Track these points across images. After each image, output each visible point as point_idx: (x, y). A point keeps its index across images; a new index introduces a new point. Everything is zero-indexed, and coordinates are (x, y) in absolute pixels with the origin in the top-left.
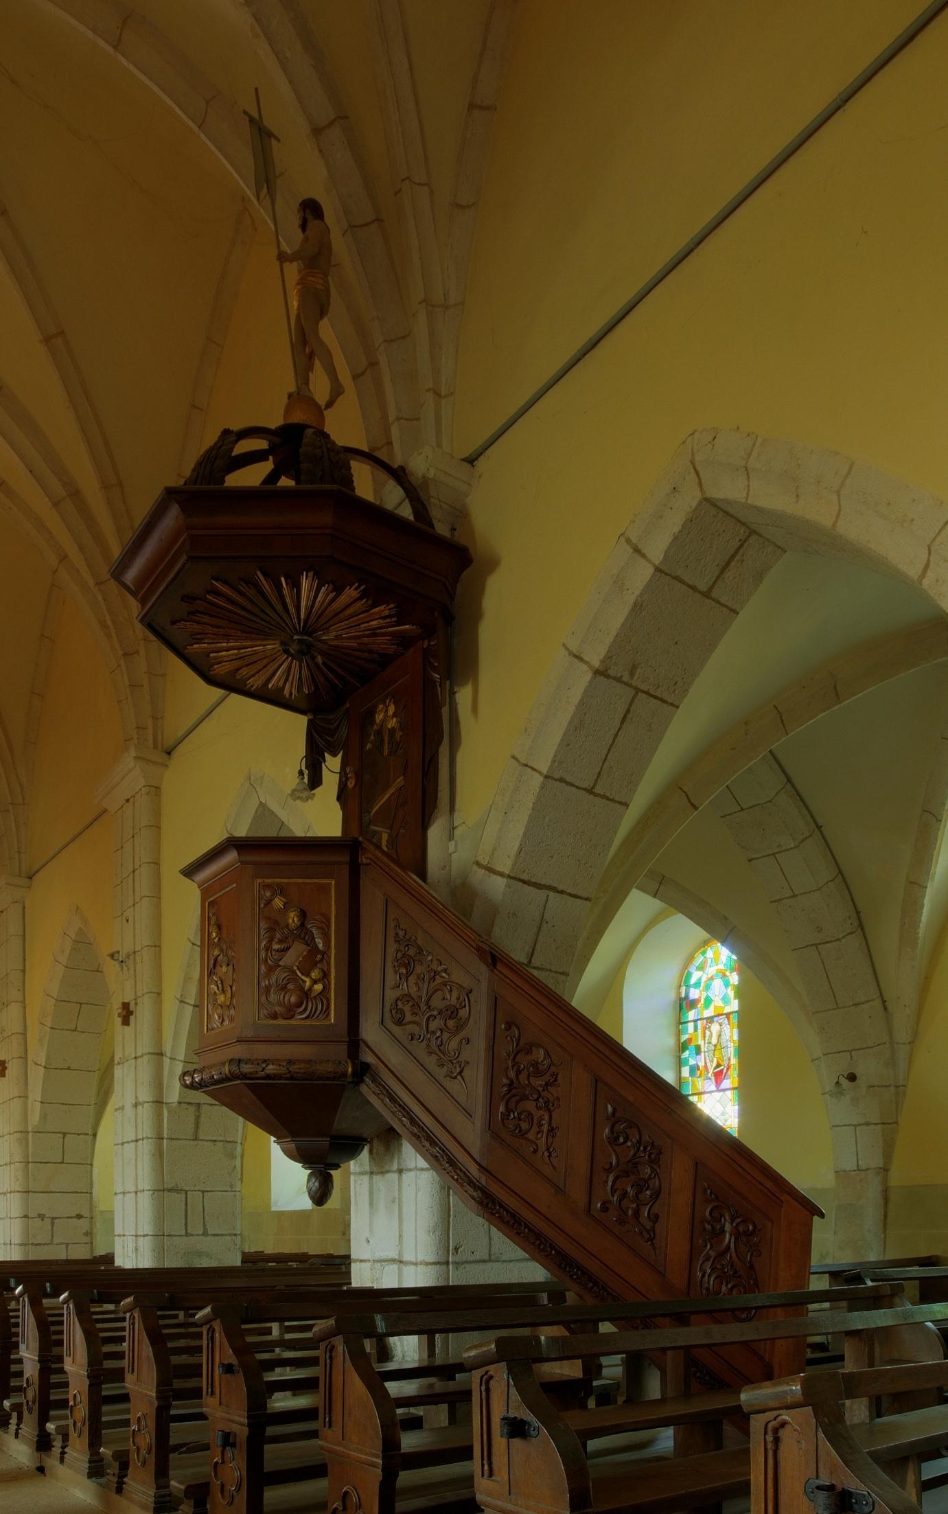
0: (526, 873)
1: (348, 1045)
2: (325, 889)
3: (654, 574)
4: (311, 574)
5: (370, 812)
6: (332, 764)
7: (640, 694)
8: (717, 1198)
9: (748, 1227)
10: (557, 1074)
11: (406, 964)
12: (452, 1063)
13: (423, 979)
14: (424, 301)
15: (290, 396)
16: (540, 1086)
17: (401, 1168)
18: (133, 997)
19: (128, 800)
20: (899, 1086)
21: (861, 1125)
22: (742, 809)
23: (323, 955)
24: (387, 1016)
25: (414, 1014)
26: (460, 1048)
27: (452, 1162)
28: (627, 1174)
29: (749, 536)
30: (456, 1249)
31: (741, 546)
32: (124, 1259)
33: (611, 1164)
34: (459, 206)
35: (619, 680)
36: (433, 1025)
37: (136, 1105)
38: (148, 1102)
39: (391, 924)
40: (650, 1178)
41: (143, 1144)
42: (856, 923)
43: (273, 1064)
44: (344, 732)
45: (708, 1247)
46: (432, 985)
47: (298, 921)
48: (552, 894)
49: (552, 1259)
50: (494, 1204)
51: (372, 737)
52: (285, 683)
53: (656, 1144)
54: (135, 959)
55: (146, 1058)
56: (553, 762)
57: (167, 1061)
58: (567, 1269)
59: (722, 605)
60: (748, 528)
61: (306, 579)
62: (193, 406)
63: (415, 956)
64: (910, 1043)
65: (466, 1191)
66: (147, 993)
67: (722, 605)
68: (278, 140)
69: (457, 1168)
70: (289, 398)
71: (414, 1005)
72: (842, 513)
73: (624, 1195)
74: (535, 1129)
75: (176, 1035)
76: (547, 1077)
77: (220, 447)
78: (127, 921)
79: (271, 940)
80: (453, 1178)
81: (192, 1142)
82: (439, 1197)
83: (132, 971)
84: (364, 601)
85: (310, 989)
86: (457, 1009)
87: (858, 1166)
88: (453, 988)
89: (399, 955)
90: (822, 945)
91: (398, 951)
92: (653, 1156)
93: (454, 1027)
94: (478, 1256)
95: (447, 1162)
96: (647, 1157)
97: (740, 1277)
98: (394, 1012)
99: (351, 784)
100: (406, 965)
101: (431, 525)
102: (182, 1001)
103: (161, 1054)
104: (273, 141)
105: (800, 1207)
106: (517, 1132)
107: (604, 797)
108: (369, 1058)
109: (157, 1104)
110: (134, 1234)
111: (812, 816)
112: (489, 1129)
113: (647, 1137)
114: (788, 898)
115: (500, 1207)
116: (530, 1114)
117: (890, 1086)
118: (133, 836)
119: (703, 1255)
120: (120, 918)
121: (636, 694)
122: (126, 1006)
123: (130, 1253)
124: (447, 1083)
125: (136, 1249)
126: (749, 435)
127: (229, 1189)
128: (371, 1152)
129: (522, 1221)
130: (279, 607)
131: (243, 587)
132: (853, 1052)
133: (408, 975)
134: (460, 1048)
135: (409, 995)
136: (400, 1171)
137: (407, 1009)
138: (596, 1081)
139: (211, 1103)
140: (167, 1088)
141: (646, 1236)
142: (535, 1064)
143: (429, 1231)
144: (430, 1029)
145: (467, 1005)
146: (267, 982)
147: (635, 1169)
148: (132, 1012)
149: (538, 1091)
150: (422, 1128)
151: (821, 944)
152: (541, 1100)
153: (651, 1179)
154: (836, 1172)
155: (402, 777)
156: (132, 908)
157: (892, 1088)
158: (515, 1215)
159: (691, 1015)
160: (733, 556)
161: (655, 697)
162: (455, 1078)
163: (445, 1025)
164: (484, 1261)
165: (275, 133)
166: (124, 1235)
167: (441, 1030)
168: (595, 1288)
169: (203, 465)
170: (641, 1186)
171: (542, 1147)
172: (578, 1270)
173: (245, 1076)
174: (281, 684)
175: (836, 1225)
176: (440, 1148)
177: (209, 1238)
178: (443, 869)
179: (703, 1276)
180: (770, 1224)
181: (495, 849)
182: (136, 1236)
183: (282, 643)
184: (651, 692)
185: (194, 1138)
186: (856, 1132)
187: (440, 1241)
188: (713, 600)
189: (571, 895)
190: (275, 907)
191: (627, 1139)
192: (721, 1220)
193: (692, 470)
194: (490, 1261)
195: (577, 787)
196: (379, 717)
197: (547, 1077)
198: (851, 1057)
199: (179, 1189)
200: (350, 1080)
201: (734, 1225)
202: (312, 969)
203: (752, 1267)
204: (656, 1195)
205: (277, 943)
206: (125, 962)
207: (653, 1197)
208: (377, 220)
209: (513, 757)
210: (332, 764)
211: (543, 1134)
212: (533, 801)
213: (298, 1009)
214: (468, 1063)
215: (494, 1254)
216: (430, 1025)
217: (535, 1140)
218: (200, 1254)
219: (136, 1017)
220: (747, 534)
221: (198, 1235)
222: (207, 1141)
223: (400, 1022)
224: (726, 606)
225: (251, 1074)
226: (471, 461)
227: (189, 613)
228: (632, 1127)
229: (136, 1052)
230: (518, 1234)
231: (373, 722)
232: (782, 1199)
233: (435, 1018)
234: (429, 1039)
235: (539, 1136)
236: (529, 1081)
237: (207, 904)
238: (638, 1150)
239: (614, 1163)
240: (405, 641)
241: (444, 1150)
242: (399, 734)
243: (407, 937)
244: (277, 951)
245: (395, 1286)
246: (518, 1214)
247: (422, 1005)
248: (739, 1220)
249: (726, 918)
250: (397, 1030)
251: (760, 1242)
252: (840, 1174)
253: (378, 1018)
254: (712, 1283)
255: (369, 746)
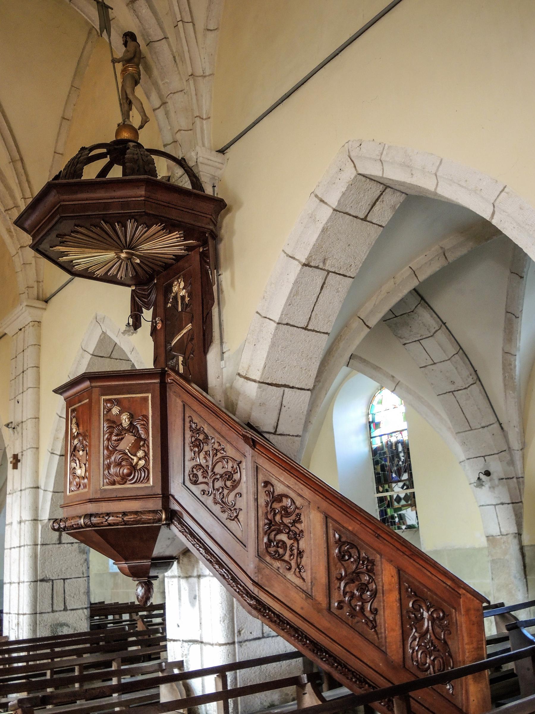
0: (269, 379)
1: (162, 499)
2: (146, 399)
3: (333, 213)
4: (133, 221)
5: (171, 344)
6: (147, 314)
7: (330, 273)
8: (415, 595)
9: (440, 614)
10: (301, 514)
11: (197, 444)
12: (231, 510)
13: (209, 454)
14: (192, 75)
15: (119, 125)
16: (290, 523)
17: (199, 574)
18: (21, 451)
19: (20, 330)
20: (519, 478)
21: (498, 504)
22: (396, 317)
23: (145, 442)
24: (187, 478)
25: (204, 477)
26: (235, 500)
27: (234, 579)
28: (353, 581)
29: (385, 189)
30: (239, 632)
31: (382, 194)
32: (9, 630)
33: (342, 574)
34: (208, 30)
35: (317, 267)
36: (218, 484)
37: (20, 522)
38: (28, 521)
39: (187, 420)
40: (369, 583)
41: (24, 550)
42: (475, 378)
43: (113, 517)
44: (153, 297)
45: (414, 630)
46: (215, 458)
47: (128, 421)
48: (286, 389)
49: (307, 647)
50: (265, 609)
51: (171, 300)
52: (117, 273)
53: (370, 558)
54: (22, 426)
55: (27, 491)
56: (282, 315)
57: (41, 492)
58: (319, 654)
59: (374, 224)
60: (384, 185)
61: (130, 222)
62: (63, 118)
63: (203, 440)
64: (521, 449)
65: (245, 600)
66: (30, 448)
67: (374, 224)
68: (112, 9)
69: (238, 584)
70: (118, 126)
71: (204, 472)
72: (439, 184)
73: (352, 596)
74: (288, 553)
75: (48, 476)
76: (293, 517)
77: (80, 157)
78: (18, 402)
79: (111, 434)
80: (235, 590)
81: (57, 546)
82: (226, 596)
83: (20, 434)
84: (165, 231)
85: (137, 464)
86: (232, 474)
87: (501, 532)
88: (229, 461)
89: (193, 439)
90: (456, 392)
91: (192, 437)
92: (369, 567)
93: (231, 486)
94: (255, 635)
95: (231, 580)
96: (365, 568)
97: (438, 651)
98: (191, 476)
99: (159, 326)
100: (198, 446)
101: (202, 189)
102: (52, 453)
103: (38, 488)
104: (110, 10)
105: (473, 597)
106: (277, 556)
107: (313, 331)
108: (176, 507)
109: (35, 521)
110: (17, 613)
111: (439, 317)
112: (258, 555)
113: (364, 555)
114: (431, 365)
115: (269, 611)
116: (284, 542)
117: (513, 478)
118: (23, 351)
119: (411, 637)
120: (13, 400)
121: (328, 274)
122: (15, 457)
123: (14, 627)
124: (229, 523)
125: (18, 624)
126: (380, 144)
127: (82, 576)
128: (178, 563)
129: (284, 619)
130: (115, 237)
131: (94, 229)
132: (486, 458)
133: (200, 451)
134: (235, 500)
135: (200, 465)
136: (199, 576)
137: (199, 474)
138: (326, 517)
139: (72, 541)
140: (41, 510)
141: (371, 625)
142: (285, 508)
143: (220, 621)
144: (215, 488)
145: (239, 472)
146: (108, 461)
147: (358, 577)
148: (20, 460)
149: (289, 527)
150: (213, 555)
151: (455, 391)
152: (291, 533)
153: (370, 583)
154: (487, 537)
155: (190, 324)
156: (21, 394)
157: (515, 480)
158: (280, 616)
159: (375, 433)
160: (377, 200)
161: (339, 274)
162: (233, 520)
163: (225, 485)
164: (259, 638)
165: (110, 6)
166: (10, 613)
167: (222, 488)
168: (339, 667)
169: (70, 167)
170: (363, 588)
171: (293, 563)
172: (326, 654)
173: (94, 525)
174: (115, 273)
175: (492, 573)
176: (226, 569)
177: (69, 612)
178: (218, 378)
179: (413, 652)
180: (454, 610)
181: (249, 366)
182: (18, 614)
183: (116, 254)
184: (336, 271)
185: (59, 542)
186: (496, 509)
187: (228, 628)
188: (369, 222)
189: (298, 389)
190: (114, 413)
191: (350, 556)
192: (420, 610)
193: (350, 160)
194: (263, 637)
195: (297, 327)
196: (175, 289)
197: (293, 517)
198: (485, 460)
199: (48, 579)
200: (165, 522)
201: (430, 613)
202: (138, 451)
203: (446, 643)
204: (374, 594)
205: (115, 436)
206: (16, 428)
207: (373, 596)
208: (165, 38)
209: (257, 313)
210: (147, 314)
211: (294, 556)
212: (271, 337)
213: (128, 478)
214: (241, 510)
215: (266, 632)
216: (215, 485)
217: (289, 561)
218: (62, 625)
219: (22, 464)
220: (384, 188)
221: (61, 611)
222: (67, 543)
223: (195, 483)
224: (376, 224)
225: (98, 524)
226: (222, 151)
227: (61, 242)
228: (353, 548)
229: (21, 487)
230: (283, 630)
231: (171, 291)
232: (460, 592)
233: (218, 480)
234: (215, 494)
235: (292, 557)
236: (282, 521)
237: (70, 410)
238: (359, 563)
239: (343, 574)
240: (189, 248)
241: (229, 571)
242: (187, 299)
243: (198, 428)
244: (115, 441)
245: (199, 668)
246: (282, 615)
247: (209, 471)
248: (432, 610)
249: (393, 377)
250: (193, 488)
251: (449, 624)
252: (490, 538)
253: (181, 480)
254: (419, 656)
255: (169, 305)
